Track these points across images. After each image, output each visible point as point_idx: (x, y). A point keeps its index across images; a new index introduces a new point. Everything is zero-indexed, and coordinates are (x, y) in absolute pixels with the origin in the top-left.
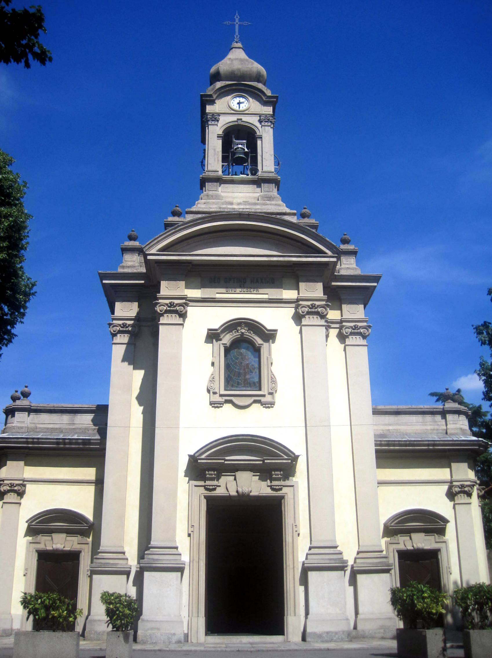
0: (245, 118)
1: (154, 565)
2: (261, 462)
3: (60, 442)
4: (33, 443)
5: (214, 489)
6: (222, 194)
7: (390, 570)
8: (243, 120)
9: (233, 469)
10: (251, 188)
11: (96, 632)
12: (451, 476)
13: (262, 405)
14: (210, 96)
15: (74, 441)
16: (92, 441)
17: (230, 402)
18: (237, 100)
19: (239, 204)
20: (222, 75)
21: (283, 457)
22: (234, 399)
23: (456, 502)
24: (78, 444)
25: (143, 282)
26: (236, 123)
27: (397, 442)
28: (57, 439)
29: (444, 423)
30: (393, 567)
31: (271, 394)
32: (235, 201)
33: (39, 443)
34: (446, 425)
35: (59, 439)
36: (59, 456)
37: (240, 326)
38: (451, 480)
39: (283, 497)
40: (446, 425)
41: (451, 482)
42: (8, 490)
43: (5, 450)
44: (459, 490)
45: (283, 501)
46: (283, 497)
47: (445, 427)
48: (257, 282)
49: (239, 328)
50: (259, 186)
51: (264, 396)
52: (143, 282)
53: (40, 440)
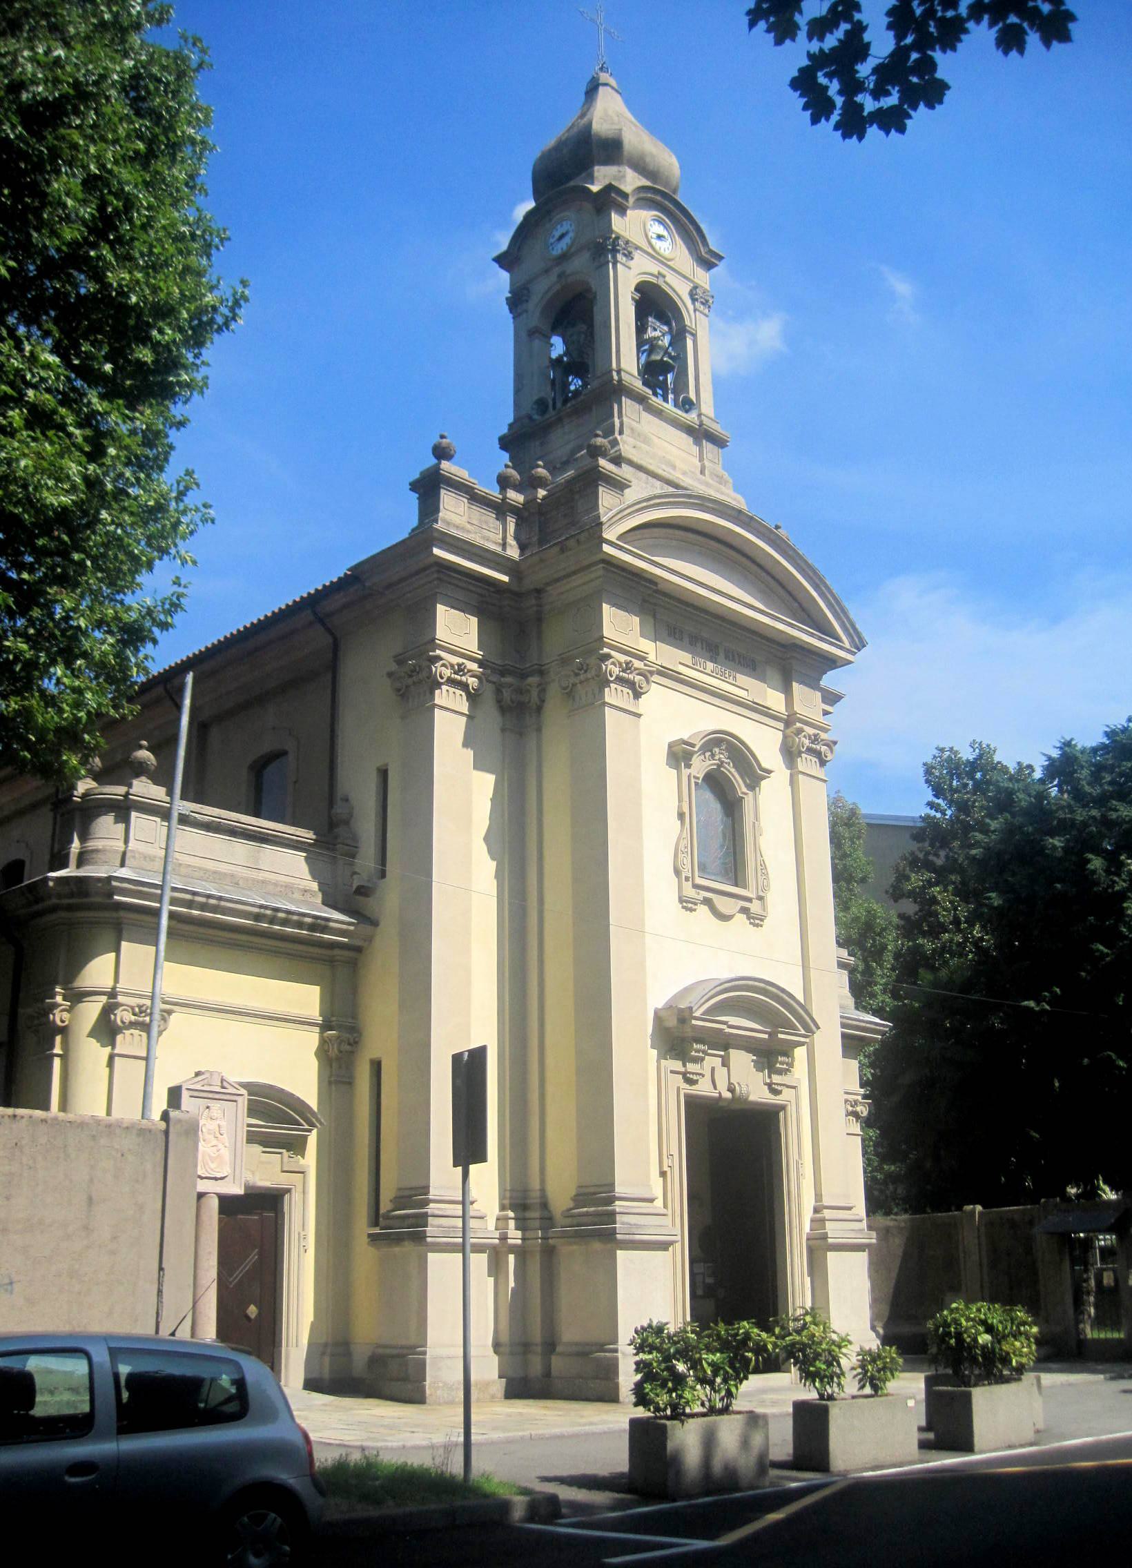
0: (672, 279)
1: (638, 1237)
2: (766, 1036)
3: (265, 916)
4: (203, 907)
5: (696, 1082)
6: (656, 440)
7: (671, 1243)
8: (667, 279)
9: (723, 1043)
10: (686, 440)
11: (445, 1384)
12: (116, 979)
13: (749, 918)
14: (625, 196)
15: (295, 918)
16: (332, 924)
17: (707, 902)
18: (660, 230)
19: (684, 473)
20: (625, 153)
21: (795, 1028)
22: (719, 901)
23: (116, 1051)
24: (300, 925)
25: (505, 579)
26: (654, 280)
27: (295, 918)
28: (261, 907)
29: (121, 835)
30: (679, 1238)
31: (761, 898)
32: (678, 463)
33: (215, 909)
34: (126, 841)
35: (266, 907)
36: (211, 942)
37: (719, 746)
38: (114, 988)
39: (783, 1108)
40: (126, 841)
41: (112, 994)
42: (131, 1023)
43: (122, 914)
44: (133, 1018)
45: (781, 1114)
46: (783, 1108)
47: (120, 845)
48: (733, 660)
49: (717, 750)
50: (697, 442)
51: (749, 900)
52: (505, 579)
53: (223, 903)
